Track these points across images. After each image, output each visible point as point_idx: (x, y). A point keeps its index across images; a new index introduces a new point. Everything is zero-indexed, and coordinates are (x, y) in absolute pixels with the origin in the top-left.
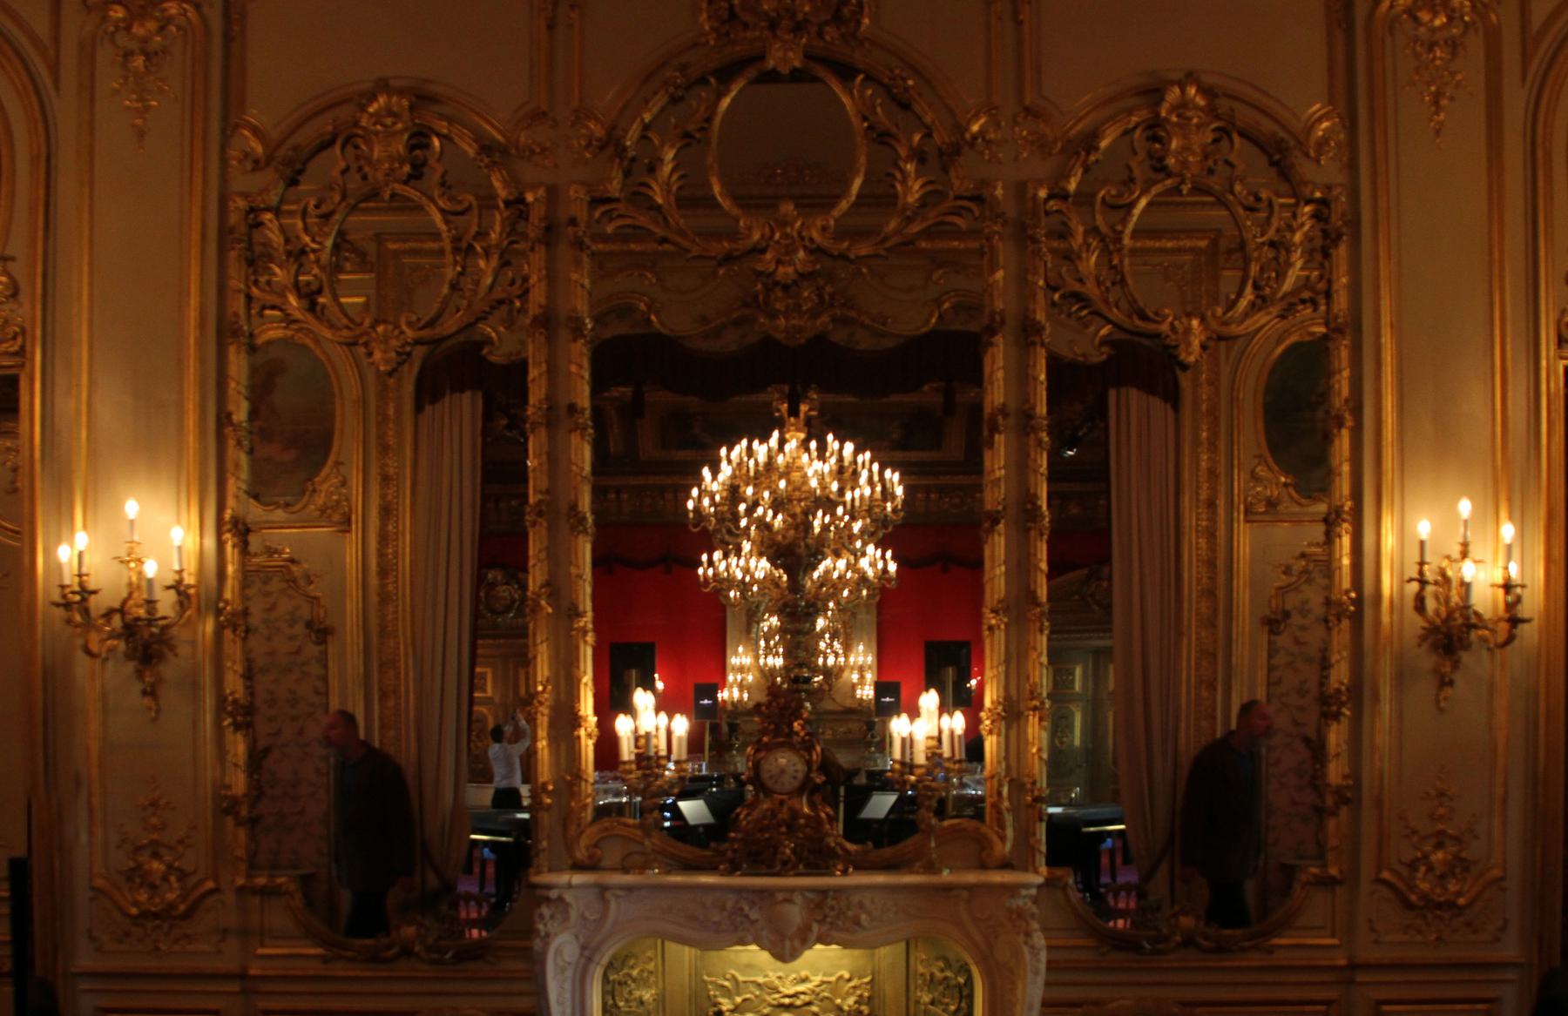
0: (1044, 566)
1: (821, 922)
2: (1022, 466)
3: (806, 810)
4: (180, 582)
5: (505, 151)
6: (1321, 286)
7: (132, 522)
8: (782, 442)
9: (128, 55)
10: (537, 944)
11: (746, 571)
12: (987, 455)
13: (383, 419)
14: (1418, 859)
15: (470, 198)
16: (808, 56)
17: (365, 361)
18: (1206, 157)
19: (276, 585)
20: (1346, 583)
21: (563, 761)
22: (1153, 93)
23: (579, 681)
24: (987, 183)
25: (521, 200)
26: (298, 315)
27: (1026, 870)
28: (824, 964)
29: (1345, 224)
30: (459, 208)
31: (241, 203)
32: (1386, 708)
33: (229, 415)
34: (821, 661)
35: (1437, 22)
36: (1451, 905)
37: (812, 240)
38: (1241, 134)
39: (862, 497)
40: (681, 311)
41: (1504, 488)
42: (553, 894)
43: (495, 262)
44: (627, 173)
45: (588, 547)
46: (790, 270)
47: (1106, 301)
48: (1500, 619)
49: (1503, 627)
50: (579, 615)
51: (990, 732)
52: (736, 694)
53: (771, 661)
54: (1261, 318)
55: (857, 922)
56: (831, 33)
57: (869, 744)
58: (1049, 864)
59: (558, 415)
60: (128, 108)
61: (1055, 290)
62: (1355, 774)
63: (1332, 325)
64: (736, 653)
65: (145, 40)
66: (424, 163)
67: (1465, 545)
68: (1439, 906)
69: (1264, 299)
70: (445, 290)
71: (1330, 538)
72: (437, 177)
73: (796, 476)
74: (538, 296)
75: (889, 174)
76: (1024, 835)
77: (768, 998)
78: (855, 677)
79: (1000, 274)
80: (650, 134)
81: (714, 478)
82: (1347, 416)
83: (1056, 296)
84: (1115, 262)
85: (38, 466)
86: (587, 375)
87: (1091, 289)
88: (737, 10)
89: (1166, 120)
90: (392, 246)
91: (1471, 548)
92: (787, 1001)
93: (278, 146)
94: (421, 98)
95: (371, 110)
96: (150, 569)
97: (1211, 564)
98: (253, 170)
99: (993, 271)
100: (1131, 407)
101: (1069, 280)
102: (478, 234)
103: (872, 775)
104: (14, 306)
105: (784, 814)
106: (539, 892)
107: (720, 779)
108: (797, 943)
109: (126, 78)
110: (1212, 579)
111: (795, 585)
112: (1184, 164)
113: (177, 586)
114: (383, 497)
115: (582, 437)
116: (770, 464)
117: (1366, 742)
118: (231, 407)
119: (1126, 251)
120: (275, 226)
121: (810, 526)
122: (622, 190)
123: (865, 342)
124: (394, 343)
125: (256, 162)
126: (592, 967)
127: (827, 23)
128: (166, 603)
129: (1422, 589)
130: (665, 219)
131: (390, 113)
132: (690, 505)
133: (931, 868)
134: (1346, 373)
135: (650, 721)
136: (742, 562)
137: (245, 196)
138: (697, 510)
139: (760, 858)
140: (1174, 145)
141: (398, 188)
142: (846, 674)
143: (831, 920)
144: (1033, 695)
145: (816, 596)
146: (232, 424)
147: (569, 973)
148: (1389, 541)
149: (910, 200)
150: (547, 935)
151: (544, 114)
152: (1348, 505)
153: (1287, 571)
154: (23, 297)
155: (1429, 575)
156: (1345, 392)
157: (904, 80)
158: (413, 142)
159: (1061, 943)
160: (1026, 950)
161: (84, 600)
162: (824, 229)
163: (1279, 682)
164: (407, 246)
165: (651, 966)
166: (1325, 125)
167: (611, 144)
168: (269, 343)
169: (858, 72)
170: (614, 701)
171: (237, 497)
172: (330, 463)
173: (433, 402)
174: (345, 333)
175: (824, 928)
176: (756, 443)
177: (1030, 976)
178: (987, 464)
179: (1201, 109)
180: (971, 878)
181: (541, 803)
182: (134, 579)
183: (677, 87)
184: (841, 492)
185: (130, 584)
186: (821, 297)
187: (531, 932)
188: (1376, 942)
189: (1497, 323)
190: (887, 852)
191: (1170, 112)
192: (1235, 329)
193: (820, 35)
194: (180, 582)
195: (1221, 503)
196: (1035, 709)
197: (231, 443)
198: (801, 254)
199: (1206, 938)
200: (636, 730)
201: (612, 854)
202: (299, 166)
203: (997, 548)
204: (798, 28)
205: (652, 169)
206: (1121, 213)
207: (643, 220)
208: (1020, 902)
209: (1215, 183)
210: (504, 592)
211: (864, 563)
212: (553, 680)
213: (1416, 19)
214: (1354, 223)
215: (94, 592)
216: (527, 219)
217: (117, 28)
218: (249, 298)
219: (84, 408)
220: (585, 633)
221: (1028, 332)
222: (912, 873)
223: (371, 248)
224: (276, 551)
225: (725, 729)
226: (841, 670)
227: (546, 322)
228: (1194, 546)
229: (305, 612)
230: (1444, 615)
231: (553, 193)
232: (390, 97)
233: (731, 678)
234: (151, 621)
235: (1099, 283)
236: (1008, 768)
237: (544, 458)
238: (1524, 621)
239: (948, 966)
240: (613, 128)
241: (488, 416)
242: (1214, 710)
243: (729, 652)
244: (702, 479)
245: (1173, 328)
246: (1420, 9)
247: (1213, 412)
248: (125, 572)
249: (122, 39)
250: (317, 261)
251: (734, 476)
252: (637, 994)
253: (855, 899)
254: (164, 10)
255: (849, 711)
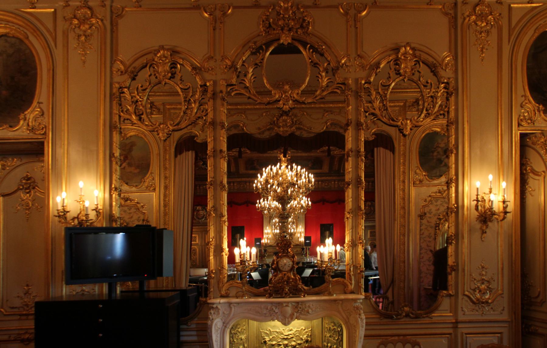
0: (363, 198)
1: (297, 312)
2: (356, 167)
3: (292, 277)
4: (97, 208)
5: (200, 69)
6: (446, 109)
7: (81, 189)
8: (281, 166)
9: (79, 36)
10: (209, 322)
11: (270, 205)
12: (346, 164)
13: (165, 160)
14: (476, 288)
15: (189, 84)
16: (293, 39)
17: (157, 137)
18: (412, 70)
19: (133, 210)
20: (453, 202)
21: (218, 262)
22: (397, 50)
23: (223, 237)
24: (346, 79)
25: (205, 85)
26: (135, 122)
27: (358, 294)
28: (298, 326)
29: (454, 90)
30: (186, 88)
31: (117, 86)
32: (466, 240)
33: (114, 154)
34: (289, 231)
35: (483, 25)
36: (487, 302)
37: (294, 97)
38: (423, 62)
39: (303, 182)
40: (253, 126)
41: (501, 171)
42: (215, 306)
43: (197, 105)
44: (238, 77)
45: (226, 195)
46: (288, 107)
47: (382, 115)
48: (502, 212)
49: (502, 215)
50: (223, 216)
51: (347, 251)
52: (266, 241)
53: (276, 231)
54: (428, 120)
55: (308, 312)
56: (300, 31)
57: (303, 254)
58: (365, 292)
59: (217, 153)
60: (80, 54)
61: (366, 112)
62: (457, 261)
63: (449, 122)
64: (266, 229)
65: (85, 31)
66: (175, 73)
67: (491, 189)
68: (483, 303)
69: (429, 114)
70: (182, 114)
71: (449, 188)
72: (179, 77)
73: (284, 176)
74: (211, 115)
75: (317, 77)
76: (358, 283)
77: (280, 336)
78: (299, 235)
79: (350, 107)
80: (245, 64)
81: (261, 177)
82: (454, 150)
83: (367, 114)
84: (385, 103)
85: (50, 171)
86: (226, 141)
87: (377, 112)
88: (271, 24)
89: (401, 58)
90: (168, 107)
91: (492, 190)
92: (286, 337)
93: (129, 67)
94: (174, 52)
95: (158, 55)
96: (87, 204)
97: (404, 199)
98: (121, 75)
99: (348, 107)
100: (381, 153)
101: (371, 109)
102: (192, 96)
103: (303, 263)
104: (43, 119)
105: (286, 278)
106: (210, 305)
107: (262, 266)
108: (289, 319)
109: (79, 44)
110: (404, 203)
111: (284, 208)
112: (405, 72)
113: (96, 210)
114: (165, 183)
115: (224, 160)
116: (277, 173)
117: (460, 251)
118: (114, 152)
119: (388, 100)
120: (128, 93)
121: (288, 192)
122: (236, 82)
123: (305, 135)
124: (166, 131)
125: (122, 72)
126: (226, 329)
127: (299, 28)
128: (92, 215)
129: (478, 203)
130: (250, 91)
131: (164, 57)
132: (254, 185)
133: (330, 294)
134: (453, 137)
135: (245, 250)
136: (268, 202)
137: (119, 83)
138: (256, 187)
139: (278, 292)
140: (402, 66)
141: (167, 80)
142: (296, 234)
143: (300, 312)
144: (360, 239)
145: (289, 212)
146: (114, 157)
147: (219, 332)
148: (466, 189)
149: (324, 84)
150: (213, 319)
151: (212, 57)
152: (454, 178)
153: (425, 201)
154: (45, 116)
155: (480, 199)
156: (453, 143)
157: (322, 46)
158: (172, 66)
159: (369, 316)
160: (359, 319)
161: (65, 214)
162: (298, 94)
163: (423, 234)
164: (172, 107)
165: (244, 328)
166: (448, 59)
167: (233, 66)
168: (131, 136)
169: (308, 44)
170: (233, 243)
171: (116, 180)
172: (149, 173)
173: (180, 154)
174: (151, 127)
175: (298, 314)
176: (273, 167)
177: (361, 328)
178: (346, 167)
179: (411, 54)
180: (342, 297)
181: (211, 277)
182: (82, 207)
183: (253, 49)
184: (297, 181)
185: (81, 209)
186: (293, 122)
187: (207, 318)
188: (464, 314)
189: (500, 120)
190: (316, 289)
191: (401, 56)
192: (420, 124)
193: (297, 32)
194: (97, 208)
195: (406, 181)
196: (361, 243)
197: (114, 163)
198: (291, 102)
199: (412, 314)
200: (240, 253)
201: (233, 292)
202: (135, 74)
203: (349, 194)
204: (290, 30)
205: (245, 76)
206: (387, 88)
207: (243, 91)
208: (357, 304)
209: (415, 78)
210: (201, 213)
211: (302, 202)
212: (215, 237)
213: (476, 24)
214: (457, 89)
215: (68, 212)
216: (207, 91)
217: (75, 27)
218: (120, 116)
219: (66, 152)
220: (225, 222)
221: (359, 125)
222: (324, 296)
223: (161, 107)
224: (133, 200)
225: (263, 251)
226: (295, 233)
227: (213, 123)
228: (399, 194)
229: (142, 217)
230: (483, 212)
231: (215, 83)
232: (164, 52)
233: (265, 236)
234: (87, 221)
235: (380, 110)
236: (353, 262)
237: (213, 167)
238: (508, 212)
239: (335, 325)
240: (233, 62)
241: (196, 159)
242: (405, 242)
243: (264, 228)
244: (258, 177)
245: (402, 124)
246: (478, 21)
247: (404, 155)
248: (79, 205)
249: (77, 30)
250: (142, 104)
251: (267, 177)
252: (240, 337)
253: (307, 305)
254: (91, 21)
255: (297, 245)
